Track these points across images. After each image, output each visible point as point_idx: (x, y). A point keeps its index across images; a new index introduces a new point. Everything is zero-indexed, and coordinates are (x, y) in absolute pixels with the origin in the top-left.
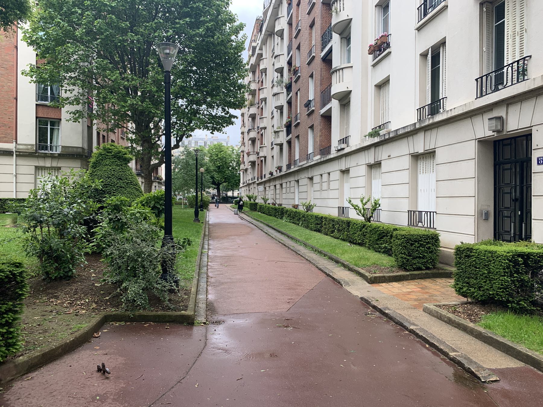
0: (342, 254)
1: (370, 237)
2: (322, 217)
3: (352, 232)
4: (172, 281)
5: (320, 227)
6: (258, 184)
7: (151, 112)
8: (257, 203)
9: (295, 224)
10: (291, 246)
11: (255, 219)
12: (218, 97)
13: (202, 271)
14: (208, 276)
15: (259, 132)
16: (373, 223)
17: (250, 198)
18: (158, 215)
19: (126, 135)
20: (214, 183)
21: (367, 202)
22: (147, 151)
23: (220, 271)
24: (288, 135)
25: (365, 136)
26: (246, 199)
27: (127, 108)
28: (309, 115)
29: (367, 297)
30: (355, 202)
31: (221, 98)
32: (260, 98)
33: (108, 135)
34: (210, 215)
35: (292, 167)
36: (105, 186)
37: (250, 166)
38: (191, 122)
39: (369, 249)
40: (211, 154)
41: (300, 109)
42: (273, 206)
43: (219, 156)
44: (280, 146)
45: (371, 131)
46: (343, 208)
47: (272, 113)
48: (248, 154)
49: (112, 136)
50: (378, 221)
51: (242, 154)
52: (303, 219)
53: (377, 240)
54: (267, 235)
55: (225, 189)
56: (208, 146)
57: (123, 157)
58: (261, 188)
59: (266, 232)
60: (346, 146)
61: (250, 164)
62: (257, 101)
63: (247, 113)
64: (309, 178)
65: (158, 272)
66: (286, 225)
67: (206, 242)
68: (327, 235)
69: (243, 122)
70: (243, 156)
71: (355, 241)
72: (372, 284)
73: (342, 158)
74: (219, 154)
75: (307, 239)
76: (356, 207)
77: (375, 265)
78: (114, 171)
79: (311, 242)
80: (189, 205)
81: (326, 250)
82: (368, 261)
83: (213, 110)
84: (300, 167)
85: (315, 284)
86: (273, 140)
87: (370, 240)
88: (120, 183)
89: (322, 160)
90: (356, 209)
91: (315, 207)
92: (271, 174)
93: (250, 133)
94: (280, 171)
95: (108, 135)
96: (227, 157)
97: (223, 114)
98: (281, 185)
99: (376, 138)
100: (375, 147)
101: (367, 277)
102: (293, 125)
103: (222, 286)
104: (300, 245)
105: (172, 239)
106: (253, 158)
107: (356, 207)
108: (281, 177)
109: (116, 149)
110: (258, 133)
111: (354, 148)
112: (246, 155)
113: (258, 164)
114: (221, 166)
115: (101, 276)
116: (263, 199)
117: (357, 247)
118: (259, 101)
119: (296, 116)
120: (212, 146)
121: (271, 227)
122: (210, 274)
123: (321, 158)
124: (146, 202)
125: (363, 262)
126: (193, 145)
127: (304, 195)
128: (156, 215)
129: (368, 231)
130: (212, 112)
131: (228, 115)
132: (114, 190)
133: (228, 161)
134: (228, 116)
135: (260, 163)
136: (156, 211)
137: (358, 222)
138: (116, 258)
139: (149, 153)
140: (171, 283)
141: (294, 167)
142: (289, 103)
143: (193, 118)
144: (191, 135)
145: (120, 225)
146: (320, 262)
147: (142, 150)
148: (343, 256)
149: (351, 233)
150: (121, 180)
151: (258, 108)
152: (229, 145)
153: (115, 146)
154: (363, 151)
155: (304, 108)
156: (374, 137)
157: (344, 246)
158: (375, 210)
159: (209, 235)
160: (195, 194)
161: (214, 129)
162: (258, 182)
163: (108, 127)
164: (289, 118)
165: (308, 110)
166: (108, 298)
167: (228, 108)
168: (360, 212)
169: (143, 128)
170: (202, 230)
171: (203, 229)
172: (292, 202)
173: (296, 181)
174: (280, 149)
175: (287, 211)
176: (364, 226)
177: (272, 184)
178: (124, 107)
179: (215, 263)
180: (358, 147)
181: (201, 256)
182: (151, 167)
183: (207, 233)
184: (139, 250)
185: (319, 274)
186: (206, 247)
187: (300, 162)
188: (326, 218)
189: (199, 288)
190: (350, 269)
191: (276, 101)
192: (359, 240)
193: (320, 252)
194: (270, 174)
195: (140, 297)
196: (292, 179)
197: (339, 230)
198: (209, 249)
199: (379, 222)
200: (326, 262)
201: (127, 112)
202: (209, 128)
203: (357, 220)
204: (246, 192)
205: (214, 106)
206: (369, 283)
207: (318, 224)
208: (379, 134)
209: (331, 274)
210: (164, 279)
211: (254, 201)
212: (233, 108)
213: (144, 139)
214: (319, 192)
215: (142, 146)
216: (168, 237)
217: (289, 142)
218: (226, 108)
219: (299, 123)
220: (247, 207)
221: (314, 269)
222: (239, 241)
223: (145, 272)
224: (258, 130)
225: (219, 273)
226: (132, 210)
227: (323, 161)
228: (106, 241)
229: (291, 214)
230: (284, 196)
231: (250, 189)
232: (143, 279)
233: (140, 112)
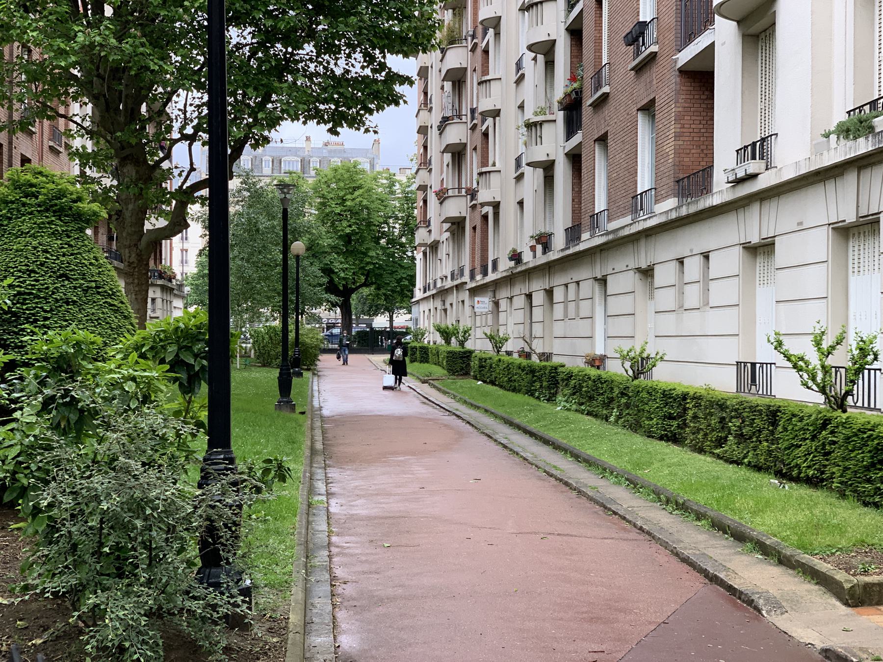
0: (754, 513)
1: (844, 459)
2: (685, 396)
3: (786, 444)
4: (235, 591)
5: (679, 427)
6: (474, 292)
7: (147, 68)
8: (471, 352)
9: (596, 416)
10: (586, 486)
11: (465, 402)
12: (353, 20)
13: (316, 562)
14: (333, 578)
15: (475, 126)
16: (856, 414)
17: (446, 335)
18: (188, 388)
19: (64, 139)
20: (331, 288)
21: (833, 348)
22: (133, 190)
23: (371, 563)
24: (570, 133)
25: (827, 136)
26: (433, 338)
27: (73, 59)
28: (639, 69)
29: (845, 649)
30: (794, 347)
31: (361, 21)
32: (480, 18)
33: (10, 143)
34: (322, 388)
35: (585, 236)
36: (20, 297)
37: (447, 234)
38: (267, 99)
39: (843, 496)
40: (323, 197)
41: (609, 49)
42: (524, 362)
43: (348, 203)
44: (545, 169)
45: (844, 117)
46: (753, 365)
47: (519, 66)
48: (442, 196)
49: (24, 146)
50: (869, 408)
51: (420, 195)
52: (623, 400)
53: (867, 469)
54: (506, 452)
55: (366, 308)
56: (313, 173)
57: (71, 208)
58: (484, 303)
59: (504, 441)
60: (763, 166)
61: (446, 226)
62: (468, 27)
63: (437, 65)
64: (639, 270)
65: (190, 563)
66: (567, 421)
67: (319, 474)
68: (701, 451)
69: (426, 94)
70: (425, 202)
71: (795, 473)
72: (856, 606)
73: (748, 205)
74: (349, 197)
75: (638, 465)
76: (797, 364)
77: (863, 546)
78: (46, 251)
79: (653, 475)
80: (258, 357)
81: (700, 499)
82: (842, 533)
83: (337, 59)
84: (611, 237)
85: (674, 607)
86: (522, 149)
87: (846, 469)
88: (65, 290)
89: (684, 212)
90: (799, 369)
91: (659, 364)
92: (516, 257)
93: (448, 128)
94: (546, 248)
95: (10, 143)
96: (372, 206)
97: (368, 72)
98: (549, 293)
99: (861, 140)
100: (860, 169)
101: (839, 584)
102: (588, 101)
103: (381, 610)
104: (615, 483)
105: (232, 461)
106: (456, 207)
107: (797, 364)
108: (549, 268)
109: (51, 186)
110: (474, 128)
111: (789, 174)
112: (433, 200)
113: (474, 228)
114: (354, 233)
115: (12, 575)
116: (491, 338)
117: (804, 491)
118: (475, 28)
119: (599, 73)
120: (327, 171)
121: (518, 427)
122: (339, 572)
123: (679, 207)
124: (152, 348)
125: (823, 539)
126: (267, 170)
127: (622, 326)
128: (181, 386)
129: (840, 438)
130: (332, 66)
131: (383, 74)
132: (45, 311)
133: (377, 218)
134: (381, 76)
135: (478, 222)
136: (183, 376)
137: (806, 410)
138: (64, 519)
139: (141, 194)
140: (232, 596)
141: (592, 236)
142: (575, 32)
143: (276, 84)
144: (266, 140)
145: (74, 417)
146: (683, 538)
147: (117, 187)
148: (758, 520)
149: (783, 445)
150: (68, 279)
151: (473, 49)
152: (378, 168)
153: (47, 176)
154: (820, 181)
155: (624, 48)
156: (855, 138)
157: (762, 486)
158: (859, 371)
159: (327, 452)
160: (277, 323)
161: (336, 121)
162: (473, 285)
163: (10, 116)
164: (573, 79)
165: (637, 53)
166: (39, 641)
167: (382, 52)
168: (814, 379)
169: (122, 119)
170: (303, 434)
171: (308, 433)
172: (584, 348)
173: (596, 279)
174: (545, 177)
175: (570, 376)
176: (826, 422)
177: (520, 289)
178: (61, 53)
179: (353, 538)
180: (803, 171)
181: (308, 514)
182: (144, 240)
183: (319, 446)
184: (138, 494)
185: (685, 576)
186: (321, 486)
187: (610, 220)
188: (697, 398)
189: (309, 614)
190: (784, 561)
191: (531, 26)
192: (809, 467)
193: (683, 507)
194: (511, 259)
195: (141, 638)
196: (583, 273)
197: (741, 437)
198: (329, 494)
199: (875, 409)
200: (702, 537)
201: (72, 70)
202: (322, 117)
203: (802, 405)
204: (435, 316)
205: (339, 46)
206: (847, 604)
207: (671, 417)
208: (871, 129)
209: (722, 575)
210: (210, 585)
211: (462, 344)
212: (397, 53)
213: (127, 152)
214: (672, 316)
215: (115, 175)
216: (219, 453)
217: (575, 158)
218: (377, 52)
219: (605, 96)
220: (437, 364)
221: (664, 557)
222: (419, 469)
223: (153, 561)
224: (473, 118)
225: (366, 567)
226: (111, 371)
227: (688, 216)
228: (33, 467)
229: (581, 387)
230: (559, 329)
231: (448, 306)
232: (149, 582)
233: (111, 70)
